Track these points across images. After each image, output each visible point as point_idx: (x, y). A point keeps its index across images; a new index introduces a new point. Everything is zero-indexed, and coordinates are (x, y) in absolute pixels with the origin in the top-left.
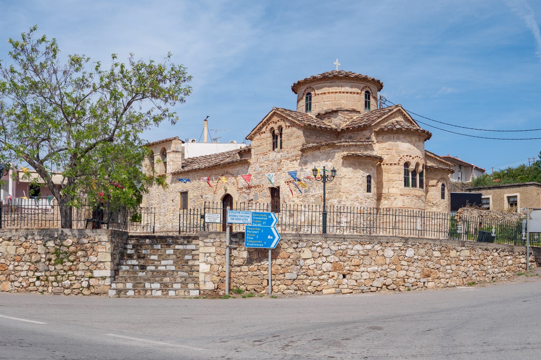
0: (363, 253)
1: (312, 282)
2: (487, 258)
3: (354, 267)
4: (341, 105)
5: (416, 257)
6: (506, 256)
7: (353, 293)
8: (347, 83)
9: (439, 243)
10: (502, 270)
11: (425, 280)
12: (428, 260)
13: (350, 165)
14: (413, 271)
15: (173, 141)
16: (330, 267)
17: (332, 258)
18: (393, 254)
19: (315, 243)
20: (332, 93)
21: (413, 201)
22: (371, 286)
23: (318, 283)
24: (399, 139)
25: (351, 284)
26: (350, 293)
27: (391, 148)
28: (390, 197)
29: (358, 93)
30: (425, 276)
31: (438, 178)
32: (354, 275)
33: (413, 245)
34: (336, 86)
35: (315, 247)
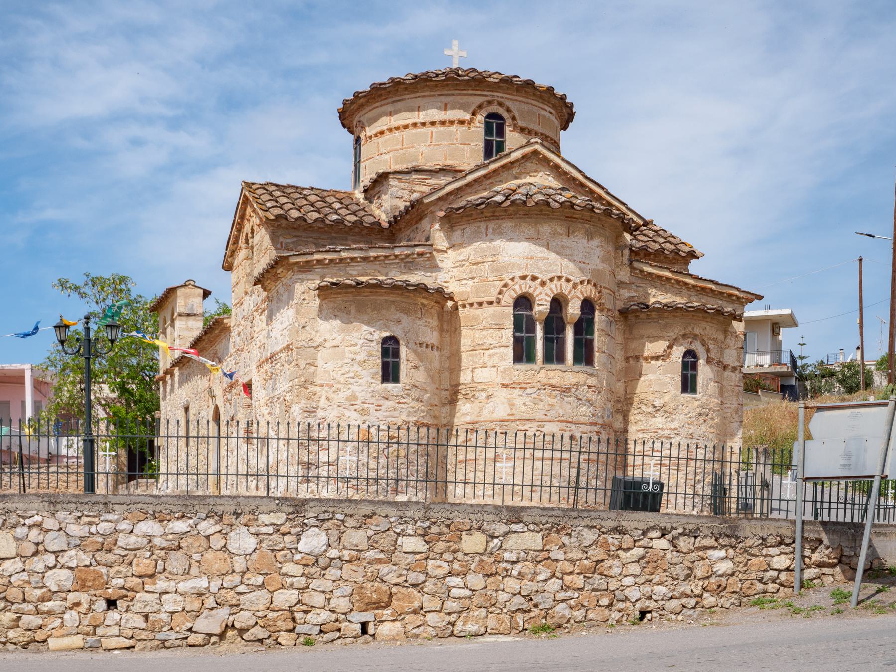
0: (165, 544)
1: (19, 618)
2: (618, 556)
3: (139, 581)
4: (417, 160)
5: (333, 553)
6: (706, 548)
7: (136, 649)
8: (432, 99)
9: (418, 515)
10: (686, 588)
11: (368, 616)
12: (379, 561)
13: (336, 313)
14: (323, 592)
15: (180, 292)
16: (66, 580)
17: (76, 558)
18: (254, 546)
19: (24, 518)
20: (397, 129)
21: (541, 400)
22: (190, 630)
23: (37, 621)
24: (499, 234)
25: (129, 625)
26: (128, 648)
27: (480, 260)
28: (477, 394)
29: (462, 123)
30: (368, 604)
31: (672, 334)
32: (139, 601)
33: (323, 520)
34: (405, 111)
35: (25, 529)
